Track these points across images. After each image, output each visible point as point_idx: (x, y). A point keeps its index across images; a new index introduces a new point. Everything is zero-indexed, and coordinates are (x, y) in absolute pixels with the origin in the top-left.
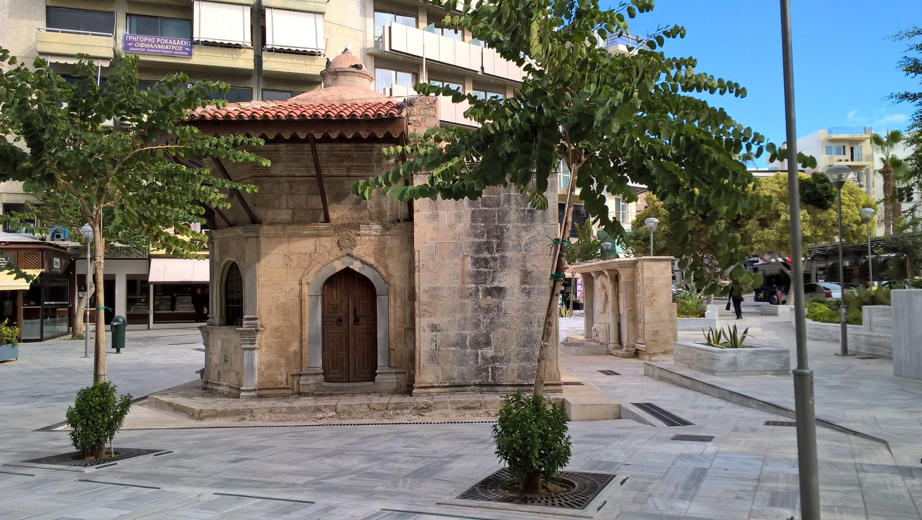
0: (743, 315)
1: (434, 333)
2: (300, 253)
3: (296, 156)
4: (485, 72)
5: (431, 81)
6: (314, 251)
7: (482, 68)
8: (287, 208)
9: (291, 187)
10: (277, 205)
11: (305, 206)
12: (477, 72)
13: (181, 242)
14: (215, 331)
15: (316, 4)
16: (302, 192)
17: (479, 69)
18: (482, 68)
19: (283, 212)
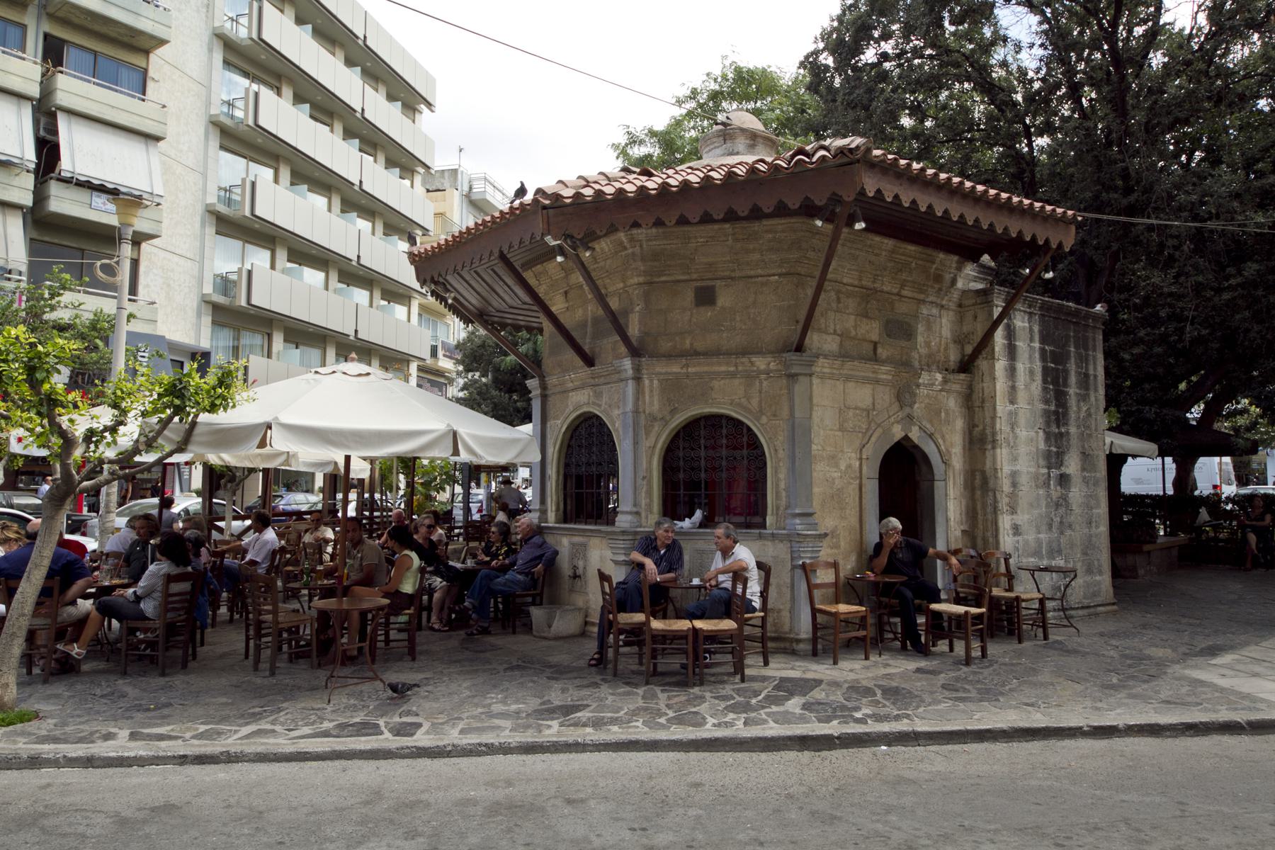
0: (418, 657)
1: (1016, 538)
2: (856, 408)
3: (853, 252)
4: (359, 336)
5: (39, 643)
6: (871, 407)
7: (356, 331)
8: (835, 333)
9: (839, 300)
10: (823, 326)
11: (853, 333)
12: (351, 260)
13: (946, 618)
14: (613, 165)
15: (156, 25)
16: (851, 310)
17: (357, 183)
18: (356, 331)
19: (829, 338)
